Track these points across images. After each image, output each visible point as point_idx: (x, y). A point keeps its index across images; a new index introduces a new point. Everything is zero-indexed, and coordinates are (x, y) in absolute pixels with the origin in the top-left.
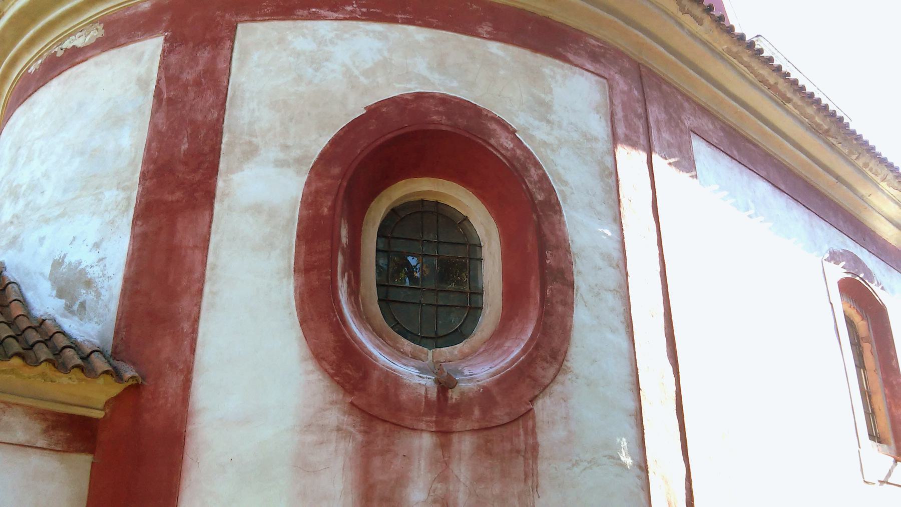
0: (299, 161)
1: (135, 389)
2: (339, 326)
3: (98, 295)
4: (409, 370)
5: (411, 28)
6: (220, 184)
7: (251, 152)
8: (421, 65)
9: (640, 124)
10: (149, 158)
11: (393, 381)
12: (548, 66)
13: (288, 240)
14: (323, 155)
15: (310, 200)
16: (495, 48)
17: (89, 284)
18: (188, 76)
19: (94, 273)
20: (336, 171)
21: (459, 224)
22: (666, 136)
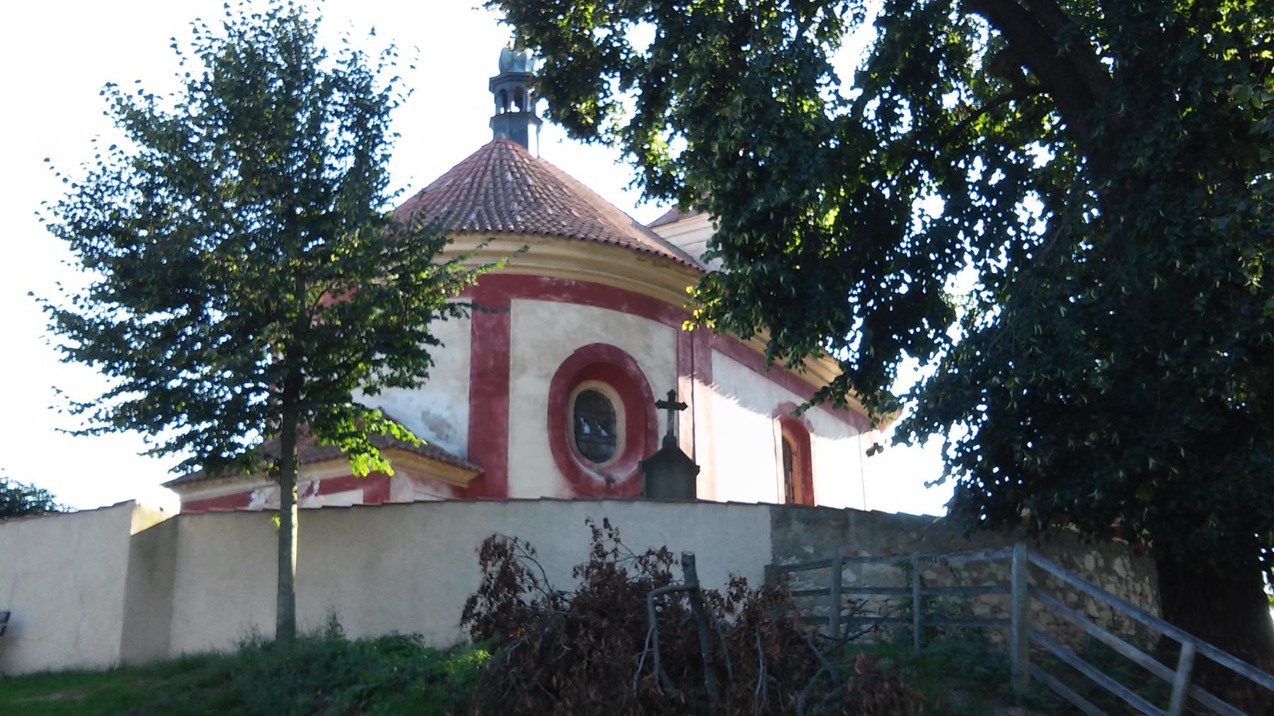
0: (546, 376)
1: (481, 477)
2: (567, 455)
3: (455, 432)
4: (592, 473)
5: (593, 308)
6: (511, 384)
7: (524, 370)
8: (597, 328)
9: (689, 350)
10: (473, 367)
11: (589, 478)
12: (652, 325)
13: (544, 414)
14: (556, 375)
15: (553, 396)
16: (629, 317)
17: (449, 426)
18: (489, 325)
19: (451, 421)
20: (563, 382)
21: (607, 402)
22: (700, 354)
